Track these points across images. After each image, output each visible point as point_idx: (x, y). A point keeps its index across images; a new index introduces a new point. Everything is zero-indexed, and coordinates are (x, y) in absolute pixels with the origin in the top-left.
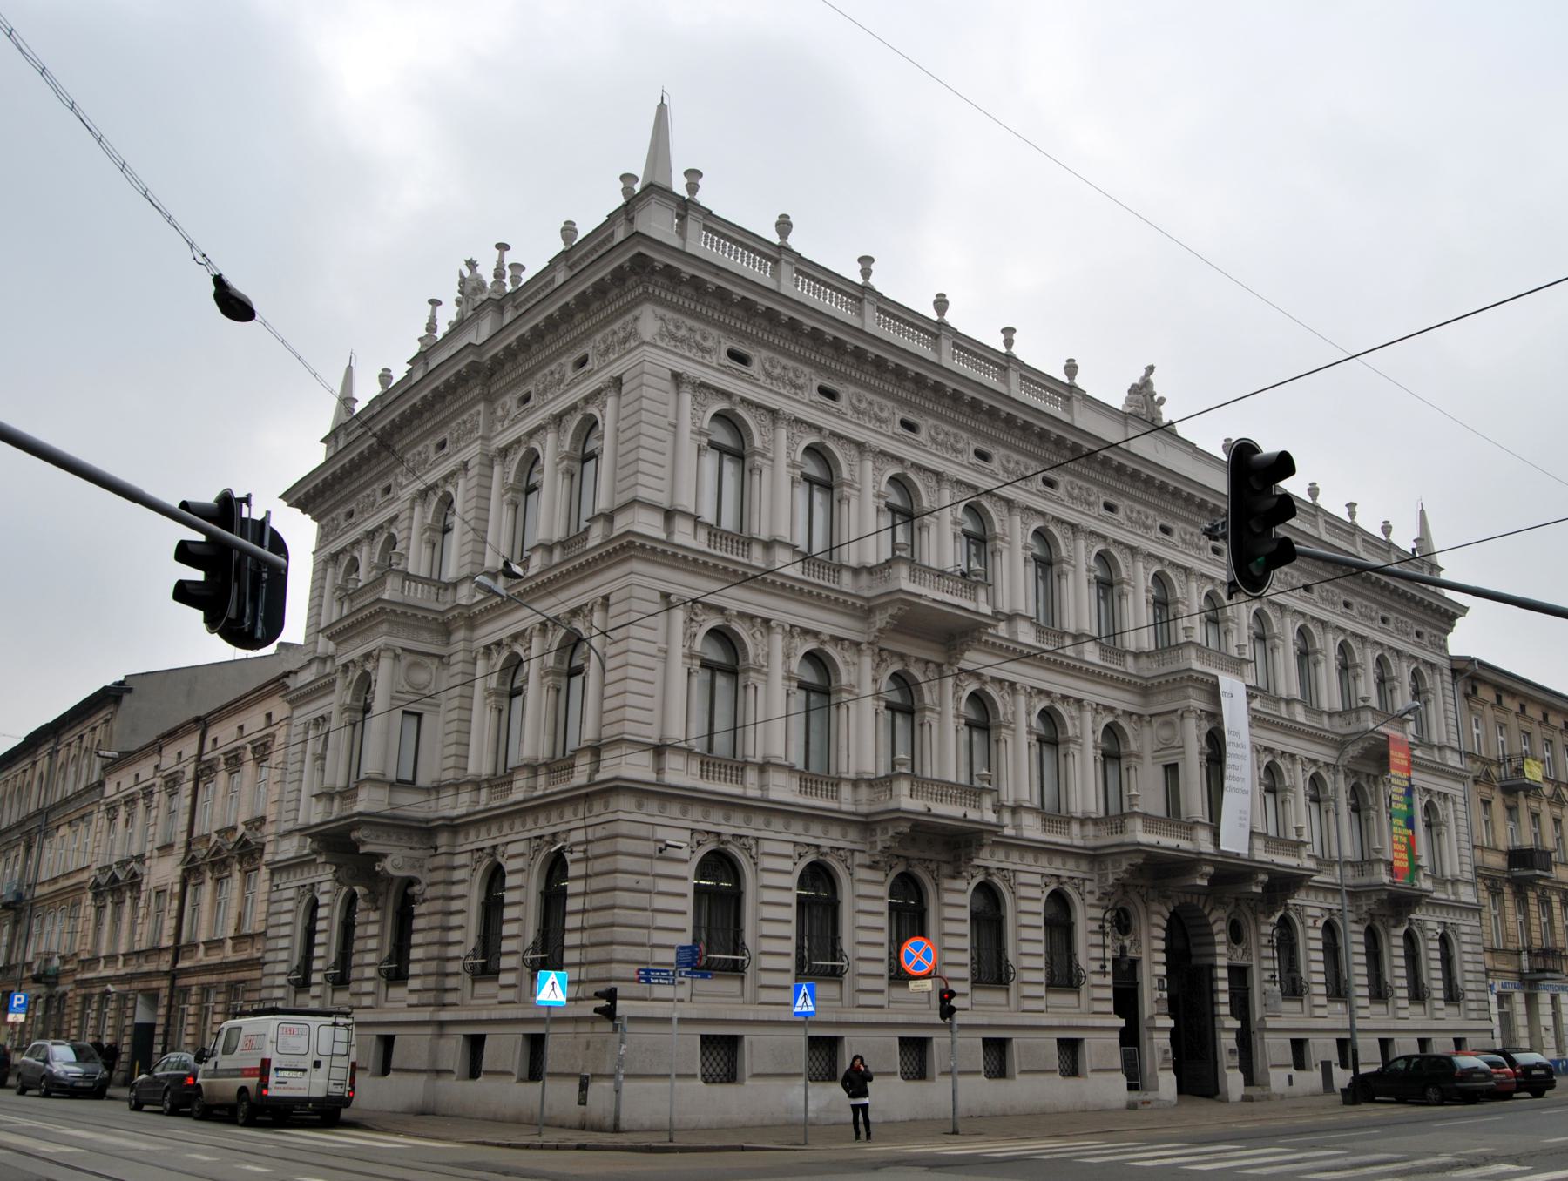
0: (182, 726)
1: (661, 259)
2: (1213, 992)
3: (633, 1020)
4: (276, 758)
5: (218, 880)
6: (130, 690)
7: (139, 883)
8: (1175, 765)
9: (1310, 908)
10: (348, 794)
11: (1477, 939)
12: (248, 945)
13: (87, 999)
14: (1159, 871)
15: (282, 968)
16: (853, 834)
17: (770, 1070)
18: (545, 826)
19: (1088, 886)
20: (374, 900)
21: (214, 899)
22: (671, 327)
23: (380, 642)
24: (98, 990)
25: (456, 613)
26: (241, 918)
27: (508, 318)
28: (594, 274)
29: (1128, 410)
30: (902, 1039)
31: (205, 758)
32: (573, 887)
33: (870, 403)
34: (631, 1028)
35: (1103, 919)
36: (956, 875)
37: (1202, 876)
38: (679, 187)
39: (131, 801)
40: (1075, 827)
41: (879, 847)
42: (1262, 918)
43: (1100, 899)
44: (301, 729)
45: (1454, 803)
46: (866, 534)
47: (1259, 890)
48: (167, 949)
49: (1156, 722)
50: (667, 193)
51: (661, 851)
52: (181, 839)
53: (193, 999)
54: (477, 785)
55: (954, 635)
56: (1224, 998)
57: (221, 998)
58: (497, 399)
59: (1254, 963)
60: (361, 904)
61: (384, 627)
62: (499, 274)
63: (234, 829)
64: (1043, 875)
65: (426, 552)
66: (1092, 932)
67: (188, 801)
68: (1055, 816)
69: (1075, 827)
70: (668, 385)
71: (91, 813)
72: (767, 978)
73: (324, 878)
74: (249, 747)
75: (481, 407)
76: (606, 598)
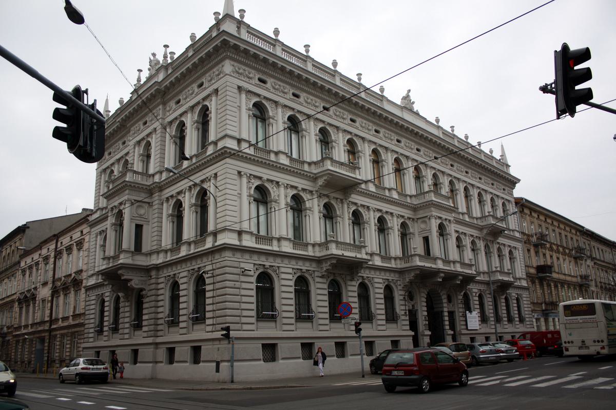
0: (49, 238)
1: (233, 41)
2: (443, 321)
3: (237, 338)
4: (86, 246)
5: (65, 294)
6: (28, 227)
7: (36, 297)
8: (428, 237)
9: (474, 289)
10: (116, 257)
11: (528, 299)
12: (78, 318)
13: (18, 342)
14: (425, 276)
15: (92, 326)
16: (314, 265)
17: (288, 356)
18: (195, 265)
19: (317, 274)
20: (127, 298)
21: (64, 302)
22: (237, 69)
23: (126, 197)
24: (21, 338)
25: (154, 185)
26: (75, 308)
27: (170, 72)
28: (206, 49)
29: (403, 105)
30: (302, 344)
31: (58, 250)
32: (208, 288)
33: (312, 100)
34: (235, 342)
35: (405, 295)
36: (352, 280)
37: (440, 278)
38: (237, 15)
39: (30, 267)
40: (393, 261)
41: (325, 269)
42: (458, 293)
43: (403, 288)
44: (95, 236)
45: (518, 251)
46: (312, 150)
47: (459, 282)
48: (47, 321)
49: (419, 221)
50: (233, 18)
51: (243, 272)
52: (50, 280)
53: (58, 339)
54: (166, 251)
55: (346, 188)
56: (447, 323)
57: (69, 338)
58: (167, 103)
59: (456, 310)
60: (122, 299)
61: (127, 192)
62: (165, 57)
63: (70, 275)
64: (383, 279)
65: (141, 164)
66: (401, 300)
67: (52, 266)
68: (386, 258)
69: (393, 261)
70: (236, 91)
71: (16, 273)
72: (285, 321)
73: (107, 292)
74: (75, 244)
75: (161, 107)
76: (216, 174)
